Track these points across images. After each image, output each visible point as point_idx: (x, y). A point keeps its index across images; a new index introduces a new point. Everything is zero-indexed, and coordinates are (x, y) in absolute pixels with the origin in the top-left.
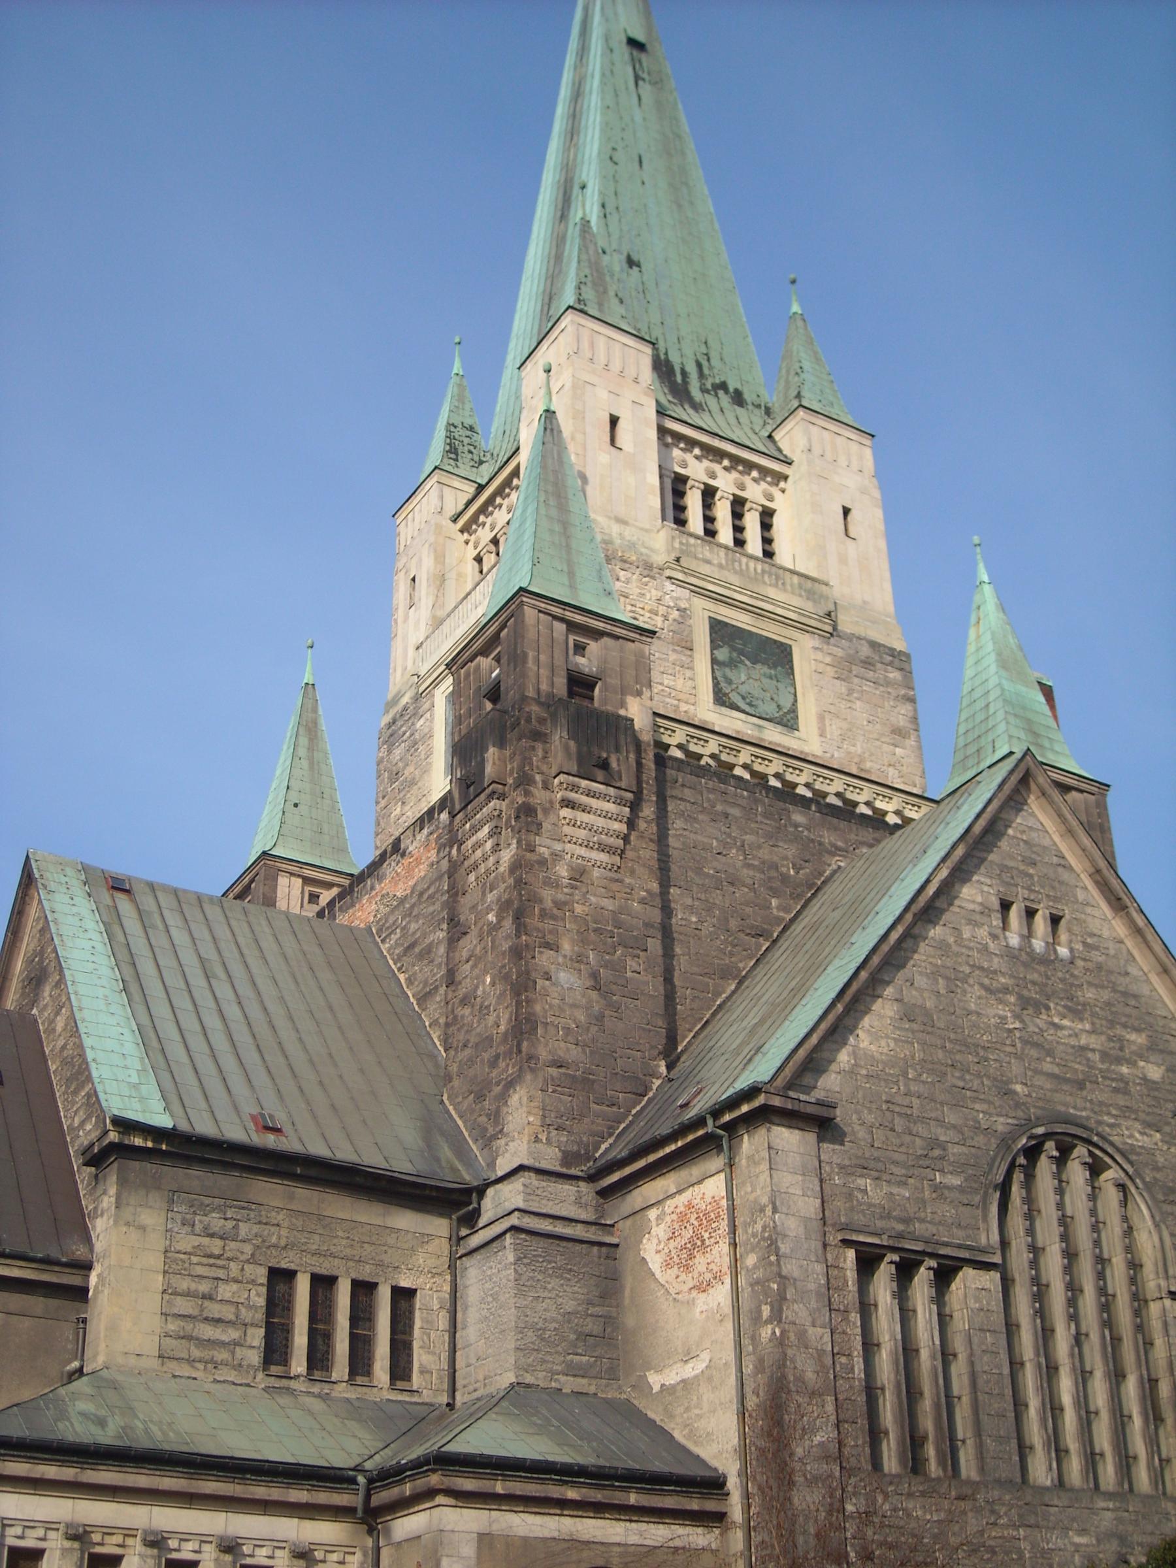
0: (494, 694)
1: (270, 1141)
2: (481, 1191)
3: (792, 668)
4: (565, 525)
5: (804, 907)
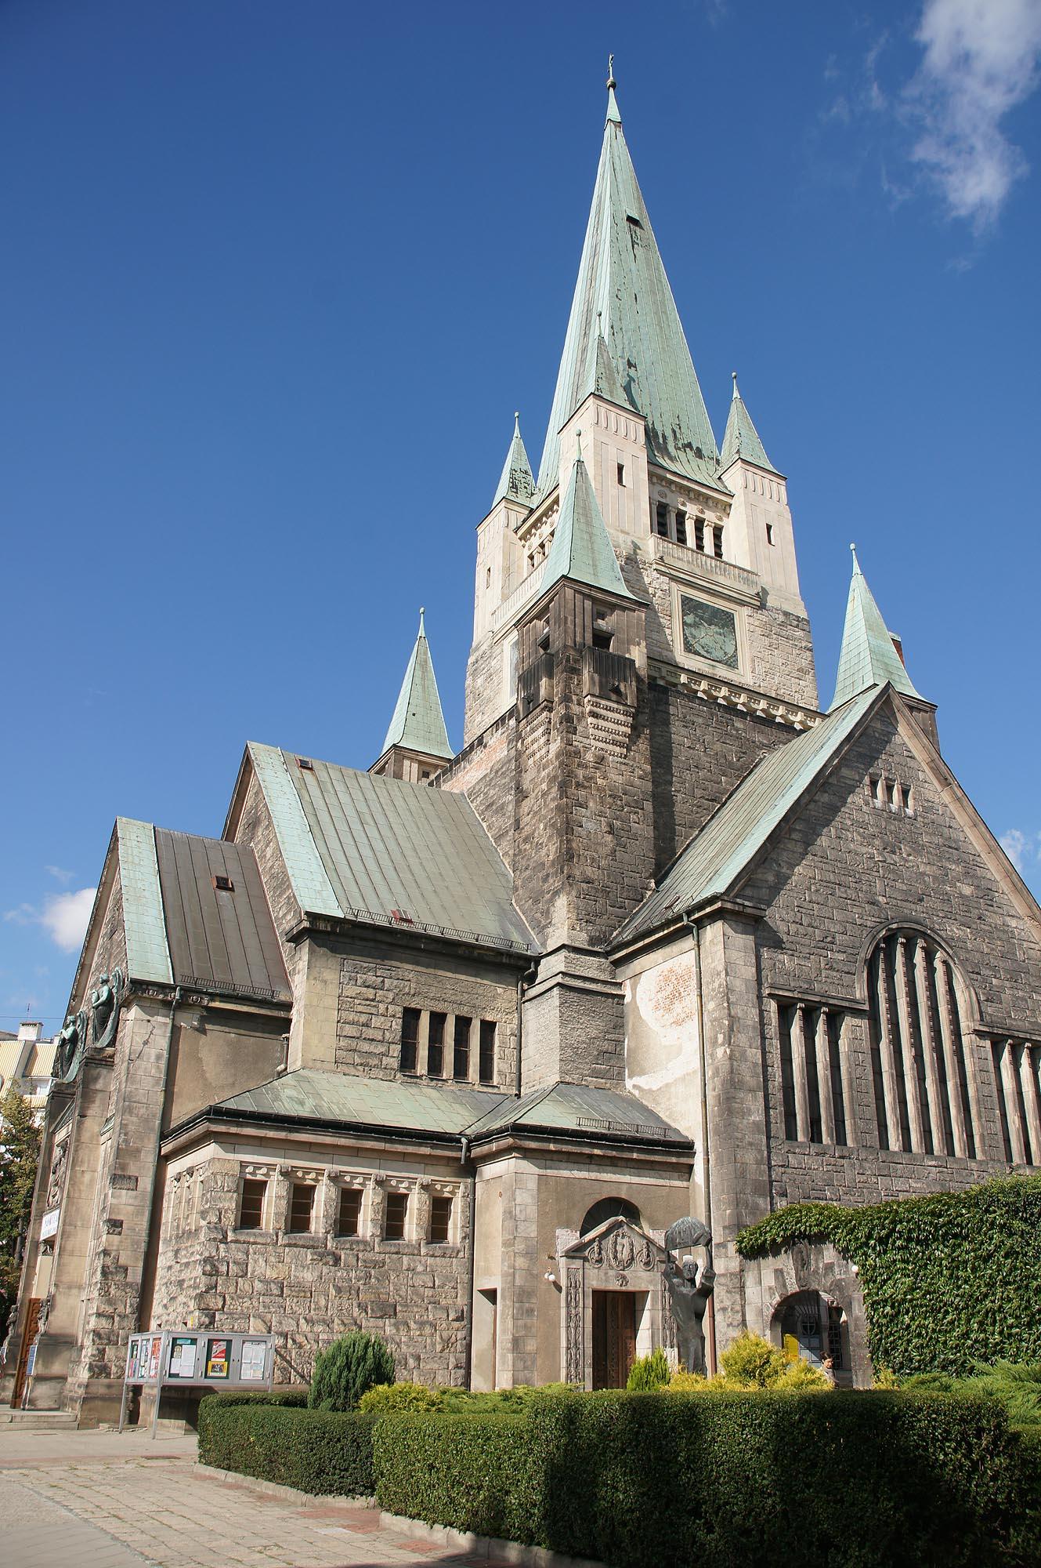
0: (545, 644)
1: (405, 926)
2: (537, 960)
3: (734, 628)
4: (591, 535)
5: (742, 782)
